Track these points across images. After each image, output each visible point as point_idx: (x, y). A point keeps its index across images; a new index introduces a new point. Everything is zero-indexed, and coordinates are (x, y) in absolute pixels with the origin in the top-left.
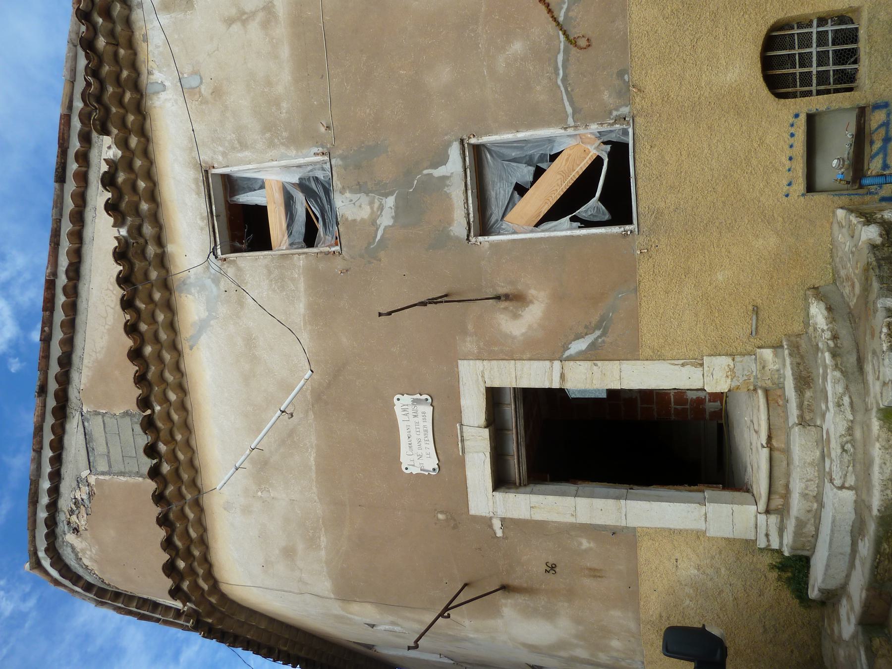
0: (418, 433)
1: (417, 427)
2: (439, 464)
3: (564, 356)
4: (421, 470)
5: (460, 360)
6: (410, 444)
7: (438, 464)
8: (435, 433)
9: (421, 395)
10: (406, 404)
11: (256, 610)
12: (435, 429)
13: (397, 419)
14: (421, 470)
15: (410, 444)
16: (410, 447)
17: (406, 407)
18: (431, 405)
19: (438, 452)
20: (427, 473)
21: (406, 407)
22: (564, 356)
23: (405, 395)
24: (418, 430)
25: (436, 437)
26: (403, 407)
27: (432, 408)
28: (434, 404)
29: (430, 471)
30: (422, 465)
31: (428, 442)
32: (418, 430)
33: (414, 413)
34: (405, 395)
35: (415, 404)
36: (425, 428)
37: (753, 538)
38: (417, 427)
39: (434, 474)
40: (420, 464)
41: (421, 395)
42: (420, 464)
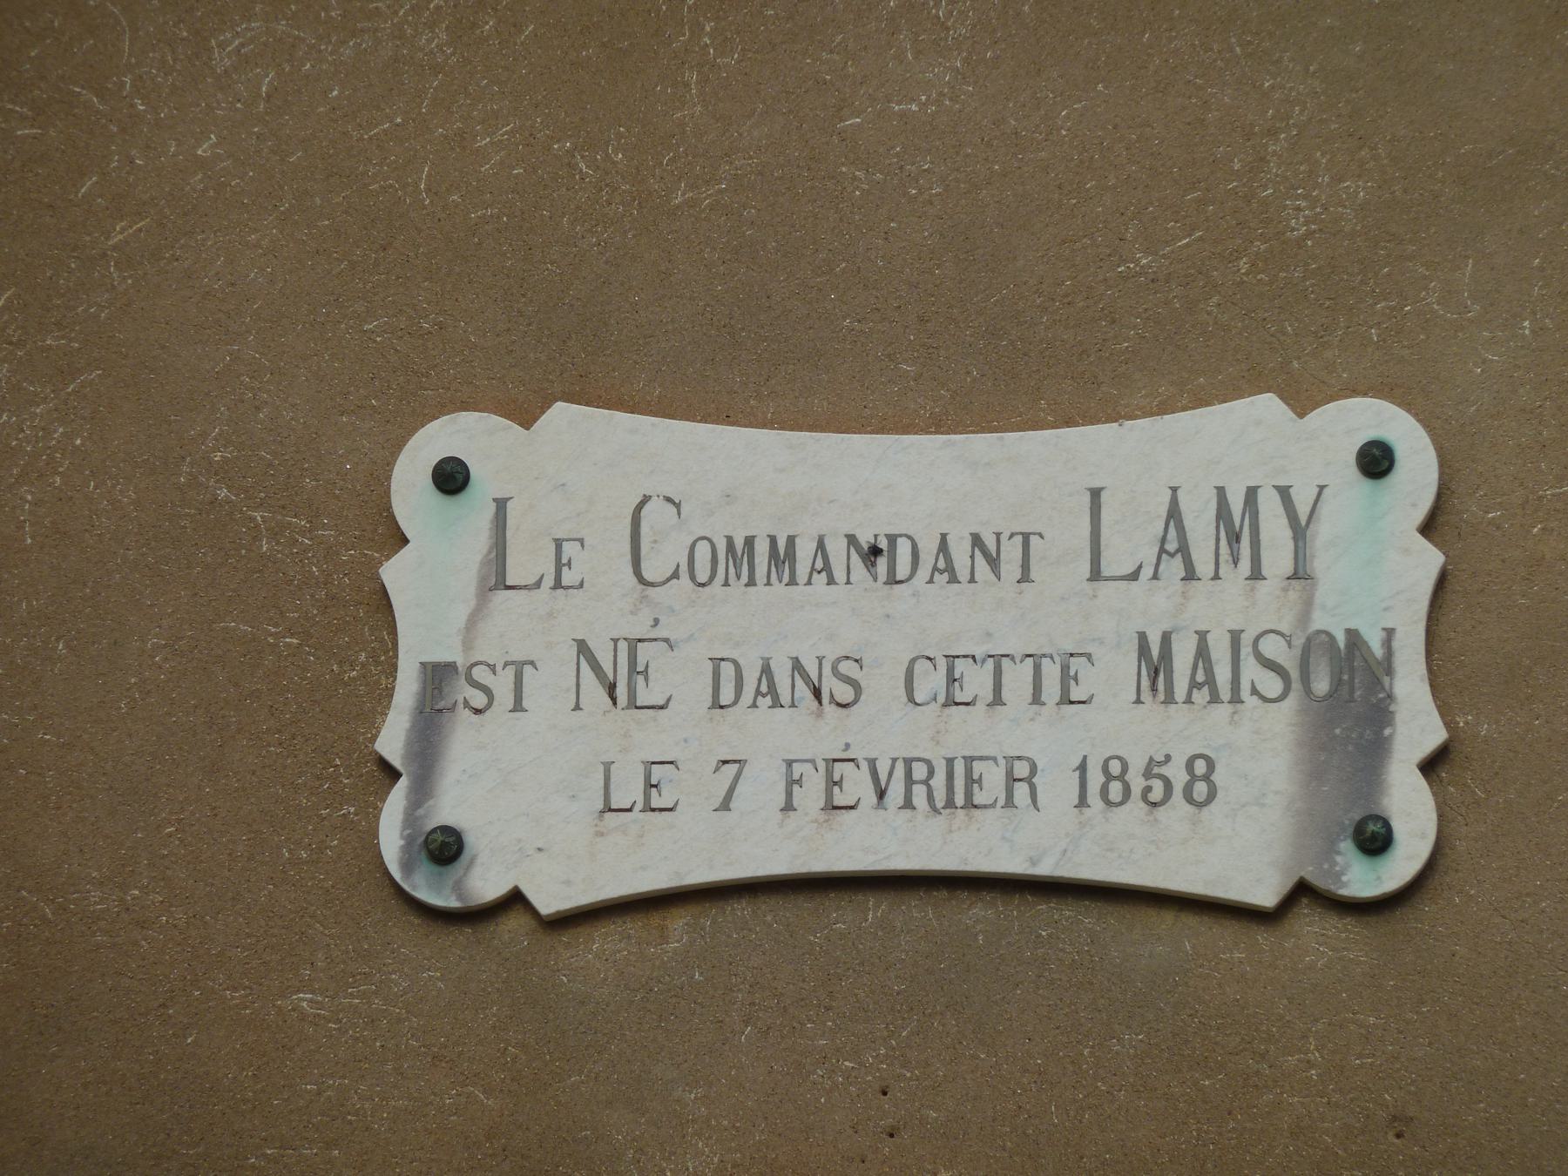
0: (931, 682)
1: (1018, 679)
2: (514, 923)
3: (1156, 661)
4: (437, 676)
5: (1182, 555)
6: (782, 557)
7: (515, 899)
8: (917, 910)
9: (1430, 767)
10: (1320, 563)
11: (1440, 746)
12: (978, 912)
13: (1114, 414)
14: (437, 676)
15: (782, 557)
16: (739, 554)
17: (1277, 558)
18: (1302, 891)
19: (678, 922)
20: (392, 742)
21: (1277, 558)
22: (1156, 661)
23: (1431, 559)
24: (977, 681)
25: (875, 908)
26: (1270, 505)
27: (1266, 896)
28: (1310, 924)
29: (423, 790)
30: (502, 685)
31: (811, 795)
32: (977, 681)
33: (1202, 653)
34: (1431, 559)
35: (1322, 686)
36: (993, 777)
37: (1021, 536)
38: (1018, 679)
39: (391, 841)
40: (519, 667)
41: (1430, 767)
42: (519, 667)
